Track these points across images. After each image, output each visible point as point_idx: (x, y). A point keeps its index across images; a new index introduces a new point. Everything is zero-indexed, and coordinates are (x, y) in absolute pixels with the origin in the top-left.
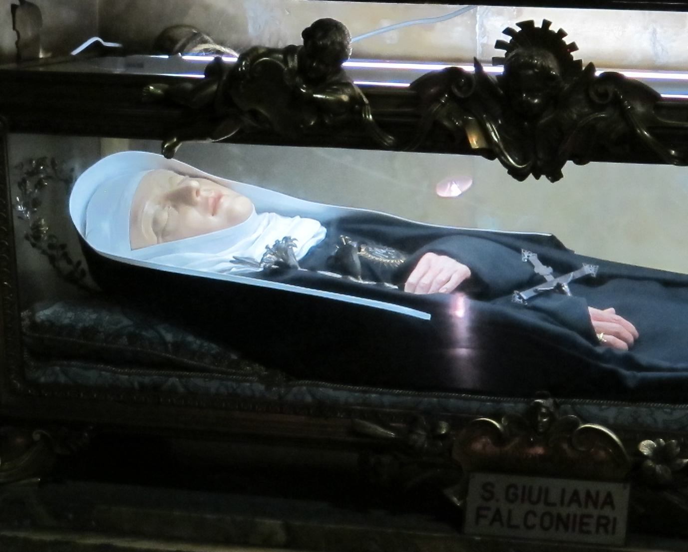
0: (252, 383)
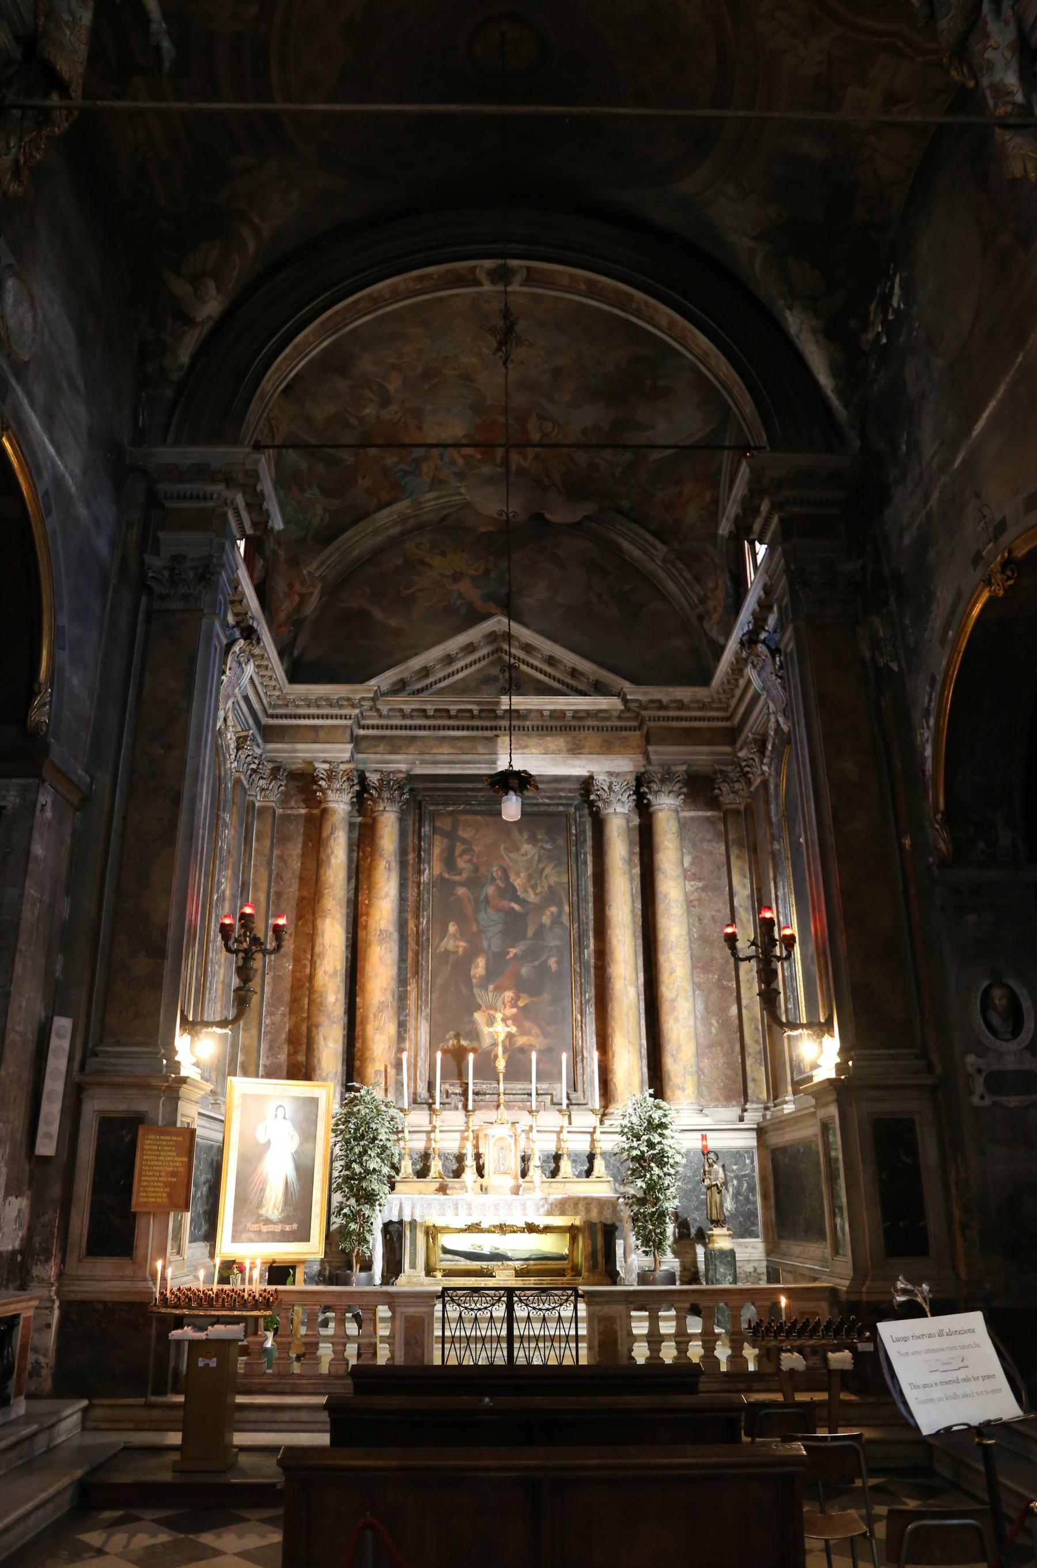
0: (468, 1262)
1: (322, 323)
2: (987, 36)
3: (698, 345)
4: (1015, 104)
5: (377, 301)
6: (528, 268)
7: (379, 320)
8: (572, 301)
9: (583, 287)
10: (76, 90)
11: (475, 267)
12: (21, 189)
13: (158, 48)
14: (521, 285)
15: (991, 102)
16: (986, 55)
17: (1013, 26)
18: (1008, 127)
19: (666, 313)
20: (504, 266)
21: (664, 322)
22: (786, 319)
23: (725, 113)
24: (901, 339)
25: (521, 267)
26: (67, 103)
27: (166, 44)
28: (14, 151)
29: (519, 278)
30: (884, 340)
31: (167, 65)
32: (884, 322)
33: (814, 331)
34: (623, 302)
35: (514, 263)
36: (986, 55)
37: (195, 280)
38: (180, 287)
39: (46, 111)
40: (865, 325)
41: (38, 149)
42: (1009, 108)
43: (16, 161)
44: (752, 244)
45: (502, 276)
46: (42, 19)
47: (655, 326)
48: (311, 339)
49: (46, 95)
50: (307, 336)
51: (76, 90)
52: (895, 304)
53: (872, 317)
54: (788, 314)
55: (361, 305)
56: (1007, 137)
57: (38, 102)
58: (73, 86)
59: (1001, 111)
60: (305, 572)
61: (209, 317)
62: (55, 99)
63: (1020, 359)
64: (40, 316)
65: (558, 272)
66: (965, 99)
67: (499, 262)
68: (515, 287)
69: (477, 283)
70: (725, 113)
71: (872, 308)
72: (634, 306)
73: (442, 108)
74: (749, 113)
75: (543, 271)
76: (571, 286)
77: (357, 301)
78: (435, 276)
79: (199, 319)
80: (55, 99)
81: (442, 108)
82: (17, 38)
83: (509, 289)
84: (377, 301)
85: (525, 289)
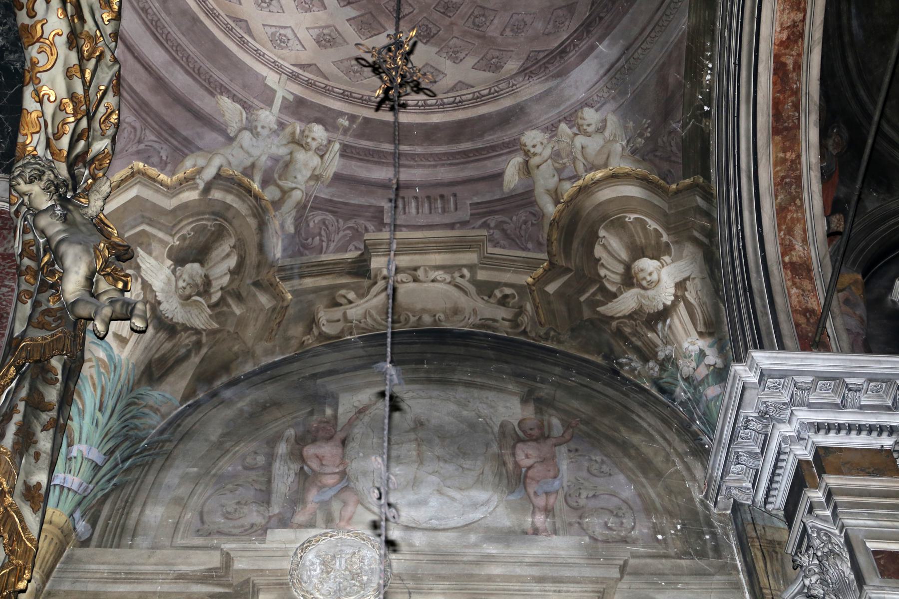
37: (629, 280)
38: (627, 302)
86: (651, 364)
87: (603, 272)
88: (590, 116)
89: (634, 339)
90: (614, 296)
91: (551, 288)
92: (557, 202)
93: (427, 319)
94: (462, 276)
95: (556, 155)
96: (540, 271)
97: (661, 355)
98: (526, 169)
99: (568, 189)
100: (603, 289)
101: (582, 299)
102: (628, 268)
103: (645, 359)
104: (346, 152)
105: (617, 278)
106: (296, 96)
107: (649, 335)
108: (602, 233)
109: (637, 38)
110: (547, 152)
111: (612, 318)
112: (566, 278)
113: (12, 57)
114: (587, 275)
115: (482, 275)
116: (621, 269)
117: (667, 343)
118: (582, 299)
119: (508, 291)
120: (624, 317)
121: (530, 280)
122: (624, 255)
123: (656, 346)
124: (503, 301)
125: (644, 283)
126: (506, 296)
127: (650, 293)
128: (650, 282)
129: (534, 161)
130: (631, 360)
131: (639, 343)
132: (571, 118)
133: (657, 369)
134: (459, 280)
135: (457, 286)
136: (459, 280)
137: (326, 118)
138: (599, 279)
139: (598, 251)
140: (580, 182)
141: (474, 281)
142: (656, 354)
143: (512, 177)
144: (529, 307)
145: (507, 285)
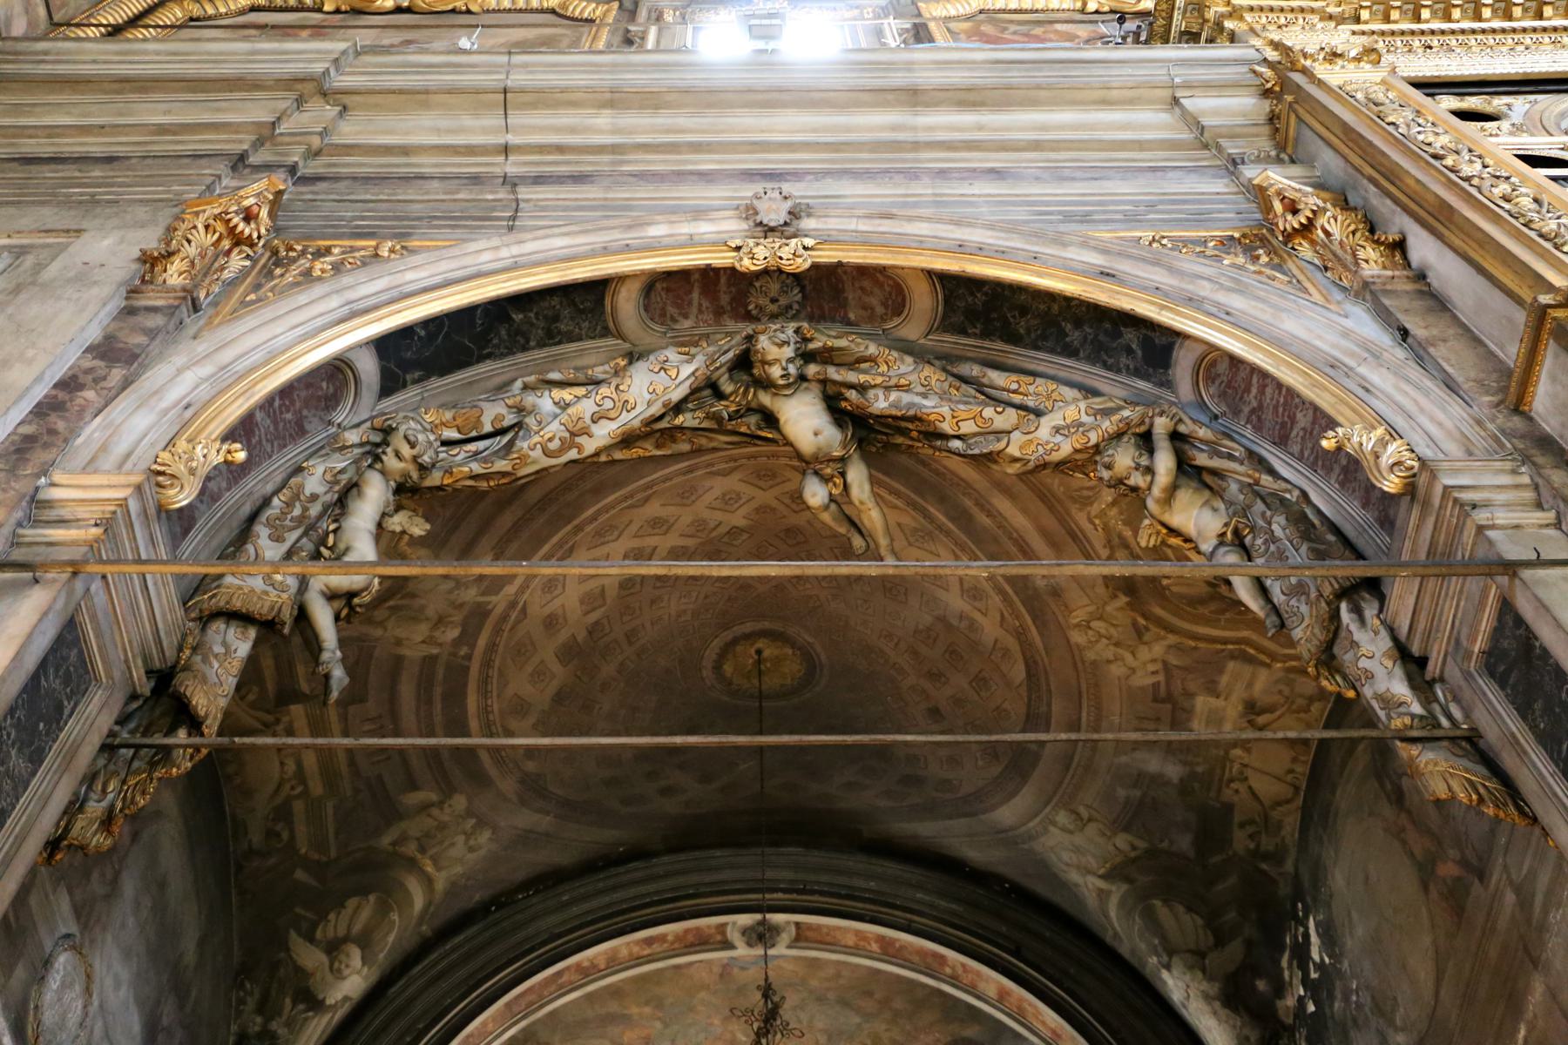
1: (508, 1005)
2: (1355, 645)
3: (1043, 1023)
4: (1413, 716)
5: (588, 973)
6: (797, 924)
7: (589, 997)
8: (858, 966)
9: (875, 947)
10: (211, 727)
11: (724, 925)
12: (109, 842)
13: (327, 677)
14: (789, 947)
15: (1382, 714)
16: (1360, 665)
17: (1384, 633)
18: (1414, 740)
19: (992, 980)
20: (763, 922)
21: (992, 992)
22: (1161, 979)
23: (1043, 737)
24: (1336, 1005)
25: (788, 923)
26: (197, 740)
27: (338, 673)
28: (110, 796)
29: (785, 938)
30: (1311, 1008)
31: (335, 695)
32: (1306, 981)
33: (1207, 997)
34: (932, 966)
35: (778, 918)
36: (1360, 665)
37: (333, 948)
38: (310, 957)
39: (167, 750)
40: (1280, 988)
41: (144, 793)
42: (1407, 720)
43: (112, 807)
44: (1101, 884)
45: (762, 936)
46: (188, 652)
47: (978, 998)
48: (490, 1027)
49: (171, 731)
50: (484, 1024)
51: (211, 727)
52: (1316, 956)
53: (1286, 974)
54: (1165, 975)
55: (565, 978)
56: (1414, 753)
57: (159, 739)
58: (208, 722)
59: (1397, 723)
60: (1261, 251)
61: (346, 998)
62: (182, 735)
63: (1522, 1033)
64: (96, 1003)
65: (839, 928)
66: (1346, 710)
67: (758, 917)
68: (780, 949)
69: (727, 945)
70: (1043, 737)
71: (1284, 963)
72: (948, 970)
73: (678, 740)
74: (1073, 736)
75: (819, 928)
76: (857, 945)
77: (559, 974)
78: (670, 938)
79: (330, 1001)
80: (182, 735)
81: (678, 740)
82: (149, 673)
83: (771, 952)
84: (588, 973)
85: (794, 952)
86: (259, 1020)
87: (332, 916)
88: (484, 837)
89: (275, 985)
90: (310, 939)
91: (300, 875)
92: (394, 844)
93: (231, 769)
94: (293, 788)
95: (442, 827)
96: (316, 857)
97: (274, 1026)
98: (425, 807)
99: (411, 849)
100: (314, 926)
101: (298, 910)
102: (346, 939)
103: (260, 1010)
104: (429, 661)
105: (330, 934)
106: (490, 611)
107: (288, 1001)
108: (372, 898)
109: (230, 386)
110: (446, 818)
111: (288, 950)
112: (314, 883)
113: (503, 332)
114: (326, 901)
115: (298, 807)
116: (341, 932)
117: (289, 1024)
118: (298, 910)
119: (285, 835)
120: (294, 963)
121: (303, 851)
122: (357, 927)
123: (280, 1015)
124: (271, 834)
125: (336, 965)
126: (278, 835)
127: (329, 977)
128: (339, 971)
129: (435, 812)
130: (252, 994)
131: (273, 993)
132: (481, 823)
133: (257, 1029)
134: (288, 786)
135: (280, 785)
136: (288, 786)
137: (468, 636)
138: (323, 916)
139: (352, 903)
140: (419, 856)
141: (288, 802)
142: (272, 1018)
143: (414, 798)
144: (272, 861)
145: (292, 831)
